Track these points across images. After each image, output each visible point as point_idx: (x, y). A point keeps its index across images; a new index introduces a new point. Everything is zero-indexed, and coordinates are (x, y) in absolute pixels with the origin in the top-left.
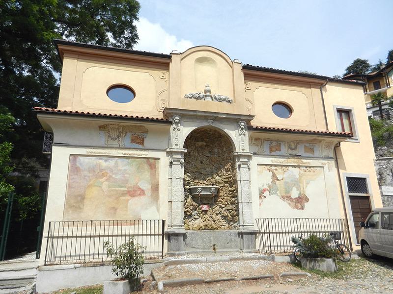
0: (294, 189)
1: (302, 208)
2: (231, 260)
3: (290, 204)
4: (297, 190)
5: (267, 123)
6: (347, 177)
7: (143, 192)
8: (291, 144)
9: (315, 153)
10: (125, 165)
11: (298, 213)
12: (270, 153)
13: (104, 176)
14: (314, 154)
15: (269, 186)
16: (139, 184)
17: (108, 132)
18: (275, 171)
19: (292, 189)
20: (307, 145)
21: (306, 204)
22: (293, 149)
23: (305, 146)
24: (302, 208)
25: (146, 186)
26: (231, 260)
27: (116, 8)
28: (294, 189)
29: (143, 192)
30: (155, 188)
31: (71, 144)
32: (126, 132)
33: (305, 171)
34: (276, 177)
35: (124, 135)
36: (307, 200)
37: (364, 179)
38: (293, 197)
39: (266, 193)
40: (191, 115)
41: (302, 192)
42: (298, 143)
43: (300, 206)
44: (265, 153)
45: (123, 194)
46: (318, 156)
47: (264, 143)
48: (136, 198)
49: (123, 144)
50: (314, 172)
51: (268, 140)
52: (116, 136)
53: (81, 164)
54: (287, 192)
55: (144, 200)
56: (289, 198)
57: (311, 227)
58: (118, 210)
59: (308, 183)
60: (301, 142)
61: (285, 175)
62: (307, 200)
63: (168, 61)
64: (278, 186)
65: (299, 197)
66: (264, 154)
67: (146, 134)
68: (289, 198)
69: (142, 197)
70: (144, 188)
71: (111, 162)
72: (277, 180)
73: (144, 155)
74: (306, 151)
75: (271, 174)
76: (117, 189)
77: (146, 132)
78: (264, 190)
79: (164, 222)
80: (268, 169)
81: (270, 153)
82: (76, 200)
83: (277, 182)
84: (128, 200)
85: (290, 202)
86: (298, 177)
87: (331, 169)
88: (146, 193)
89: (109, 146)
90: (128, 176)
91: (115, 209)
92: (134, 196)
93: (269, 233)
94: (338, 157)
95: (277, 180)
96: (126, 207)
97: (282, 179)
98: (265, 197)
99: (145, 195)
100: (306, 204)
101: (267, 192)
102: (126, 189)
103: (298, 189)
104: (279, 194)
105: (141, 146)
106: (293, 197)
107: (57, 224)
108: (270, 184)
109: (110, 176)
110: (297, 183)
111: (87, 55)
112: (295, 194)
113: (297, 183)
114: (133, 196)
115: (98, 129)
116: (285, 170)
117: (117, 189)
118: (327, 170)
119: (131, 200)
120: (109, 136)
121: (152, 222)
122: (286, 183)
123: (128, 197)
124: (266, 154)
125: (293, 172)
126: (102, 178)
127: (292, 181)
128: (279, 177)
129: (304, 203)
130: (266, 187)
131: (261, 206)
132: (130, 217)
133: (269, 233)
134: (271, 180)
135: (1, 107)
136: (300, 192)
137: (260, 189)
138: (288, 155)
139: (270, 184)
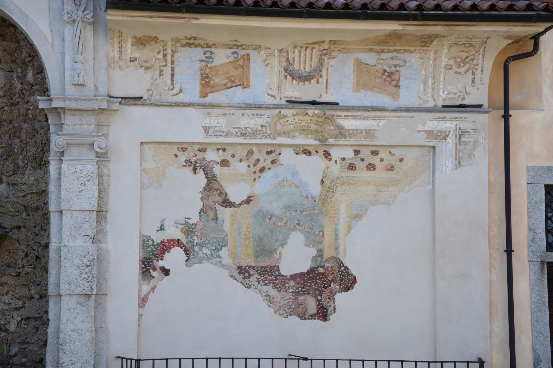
0: (297, 239)
1: (323, 314)
3: (270, 300)
4: (307, 245)
6: (547, 186)
8: (294, 55)
11: (305, 335)
12: (204, 95)
14: (395, 96)
15: (189, 229)
18: (217, 170)
20: (370, 58)
21: (341, 299)
22: (306, 78)
23: (359, 63)
24: (323, 314)
28: (297, 239)
33: (352, 167)
36: (348, 282)
38: (287, 269)
39: (174, 258)
41: (328, 253)
42: (325, 54)
43: (312, 305)
44: (181, 98)
46: (415, 103)
47: (177, 55)
51: (191, 43)
54: (263, 249)
56: (270, 274)
60: (336, 45)
61: (262, 186)
62: (348, 282)
64: (227, 227)
65: (312, 270)
66: (175, 99)
68: (270, 274)
72: (227, 203)
74: (361, 85)
75: (201, 179)
78: (165, 247)
79: (84, 236)
80: (188, 162)
81: (204, 95)
83: (225, 213)
85: (273, 292)
86: (315, 189)
87: (471, 156)
94: (514, 98)
95: (227, 203)
97: (248, 201)
98: (166, 272)
100: (341, 299)
101: (177, 253)
103: (314, 238)
106: (287, 269)
108: (195, 219)
111: (474, 109)
112: (295, 258)
113: (310, 216)
122: (265, 216)
124: (186, 100)
125: (295, 174)
127: (287, 207)
128: (236, 193)
129: (333, 293)
130: (175, 233)
131: (147, 305)
134: (200, 205)
136: (320, 252)
137: (145, 242)
138: (283, 102)
139: (195, 219)
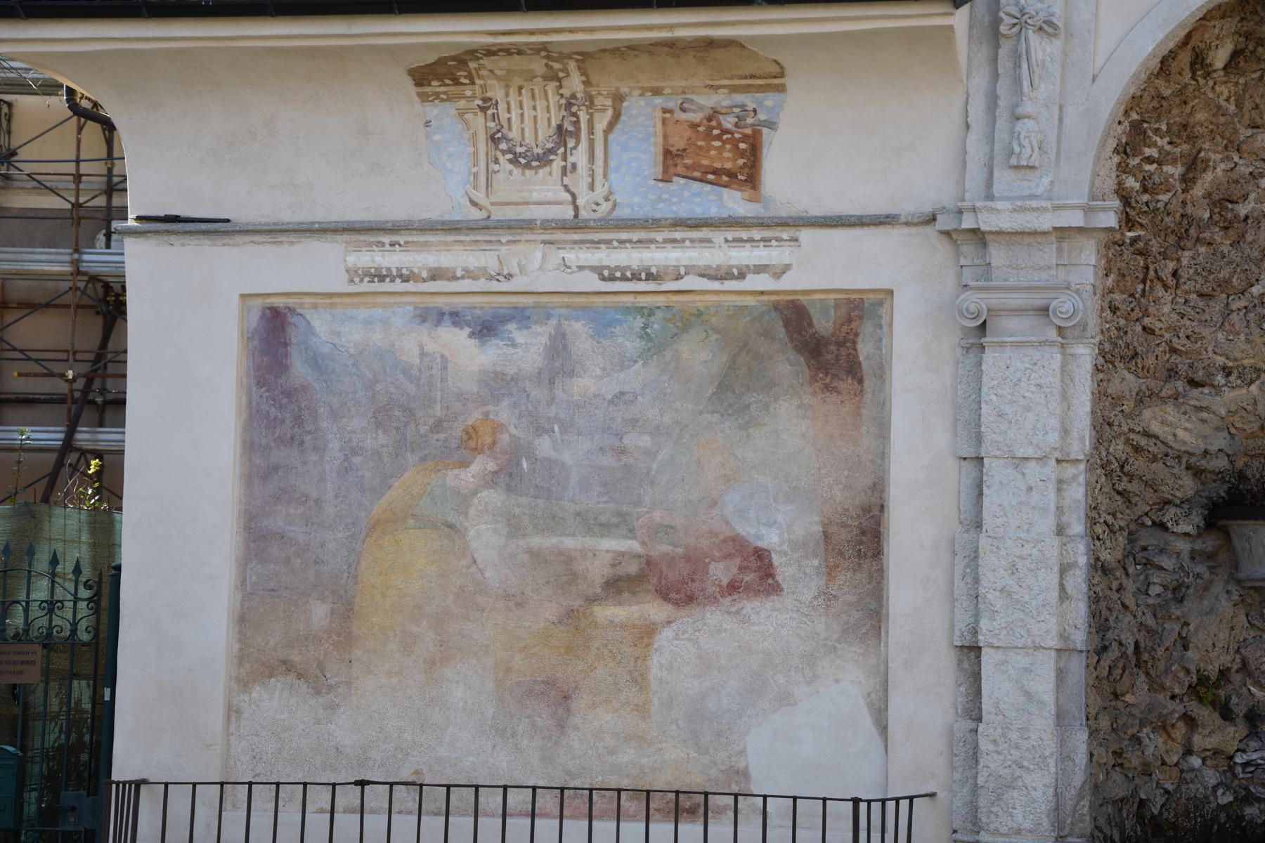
7: (757, 572)
10: (624, 363)
13: (477, 450)
17: (487, 104)
29: (757, 572)
30: (861, 540)
31: (240, 213)
32: (618, 99)
35: (601, 124)
40: (762, 86)
45: (619, 585)
48: (713, 617)
49: (600, 191)
52: (545, 134)
53: (316, 362)
55: (770, 624)
58: (580, 703)
67: (770, 100)
69: (754, 608)
70: (770, 539)
71: (520, 337)
73: (760, 269)
77: (773, 79)
82: (298, 614)
84: (647, 633)
88: (785, 570)
89: (498, 214)
90: (645, 441)
91: (560, 698)
92: (690, 599)
93: (78, 161)
96: (640, 680)
99: (776, 589)
102: (634, 546)
105: (734, 202)
109: (518, 451)
115: (412, 89)
119: (668, 633)
120: (494, 140)
123: (655, 610)
126: (464, 464)
132: (673, 764)
133: (78, 161)
135: (1262, 758)
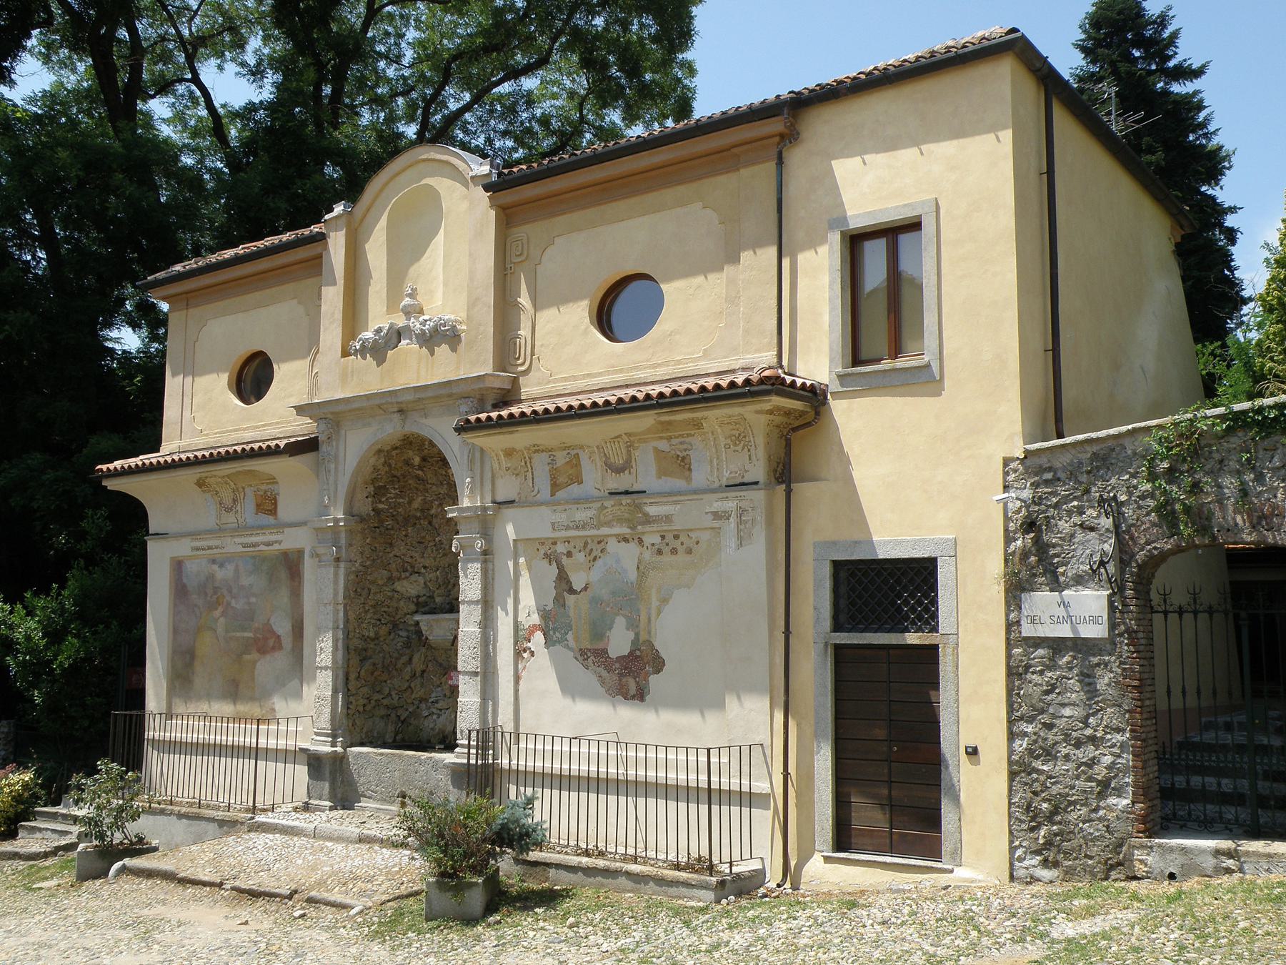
0: (620, 622)
2: (362, 840)
3: (602, 681)
5: (565, 379)
9: (694, 474)
14: (689, 479)
16: (272, 622)
19: (613, 622)
21: (653, 680)
22: (619, 470)
25: (282, 627)
26: (362, 840)
27: (606, 141)
28: (620, 622)
34: (569, 582)
36: (658, 664)
37: (837, 565)
41: (643, 637)
50: (689, 551)
56: (601, 654)
57: (236, 731)
59: (665, 601)
61: (595, 575)
62: (658, 664)
63: (319, 250)
65: (631, 653)
72: (572, 591)
75: (553, 571)
76: (238, 634)
83: (571, 599)
84: (255, 662)
85: (604, 673)
86: (633, 575)
87: (750, 535)
95: (572, 591)
97: (585, 589)
98: (532, 654)
103: (633, 624)
104: (572, 643)
107: (724, 752)
110: (629, 599)
112: (619, 643)
113: (629, 599)
114: (263, 651)
116: (594, 554)
117: (238, 634)
118: (734, 540)
121: (714, 753)
122: (595, 601)
129: (648, 675)
136: (637, 635)
